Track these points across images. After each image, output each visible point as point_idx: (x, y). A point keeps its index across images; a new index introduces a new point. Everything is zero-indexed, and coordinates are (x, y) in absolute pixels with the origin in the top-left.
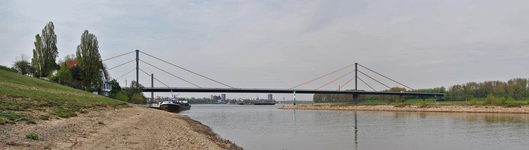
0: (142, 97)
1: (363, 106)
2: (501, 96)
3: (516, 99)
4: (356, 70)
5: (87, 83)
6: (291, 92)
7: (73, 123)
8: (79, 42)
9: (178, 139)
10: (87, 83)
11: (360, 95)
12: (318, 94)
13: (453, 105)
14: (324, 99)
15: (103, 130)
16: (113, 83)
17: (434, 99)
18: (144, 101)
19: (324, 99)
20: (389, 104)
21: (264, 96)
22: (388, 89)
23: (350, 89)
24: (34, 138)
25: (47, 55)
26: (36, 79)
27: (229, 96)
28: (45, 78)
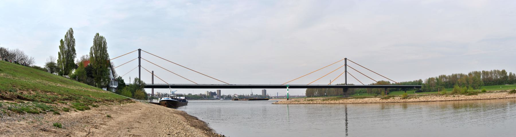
0: (143, 93)
1: (352, 100)
2: (464, 86)
3: (474, 88)
4: (346, 65)
5: (98, 80)
6: (284, 87)
7: (87, 115)
8: (92, 44)
9: (176, 133)
10: (98, 80)
11: (350, 89)
12: (310, 89)
13: (429, 95)
14: (316, 93)
15: (111, 123)
16: (119, 80)
17: (413, 91)
18: (145, 97)
19: (316, 93)
20: (376, 97)
21: (258, 92)
22: (375, 82)
23: (341, 83)
24: (58, 126)
25: (68, 56)
26: (60, 77)
27: (225, 92)
28: (67, 76)
